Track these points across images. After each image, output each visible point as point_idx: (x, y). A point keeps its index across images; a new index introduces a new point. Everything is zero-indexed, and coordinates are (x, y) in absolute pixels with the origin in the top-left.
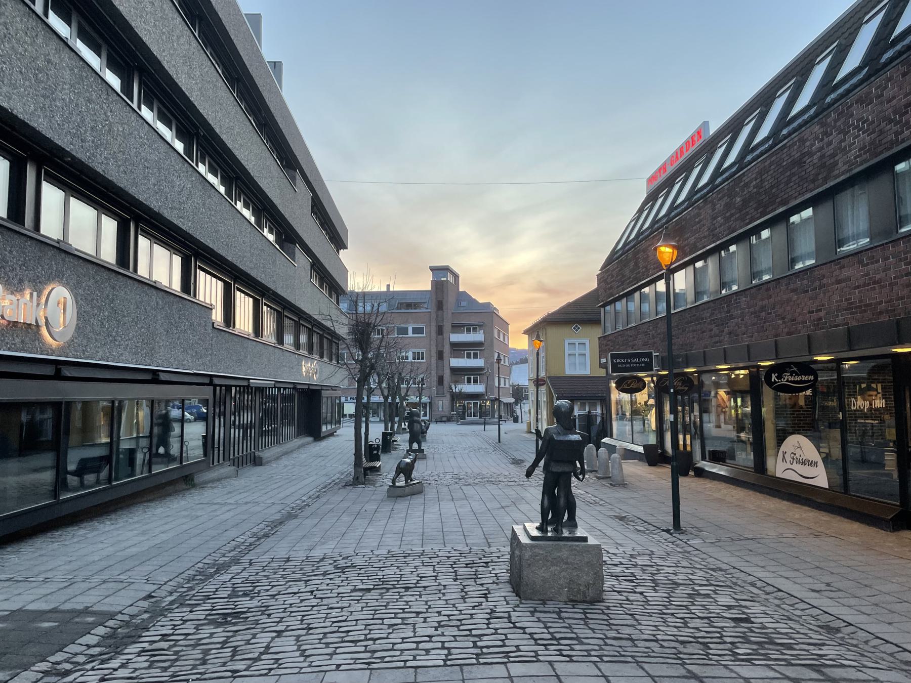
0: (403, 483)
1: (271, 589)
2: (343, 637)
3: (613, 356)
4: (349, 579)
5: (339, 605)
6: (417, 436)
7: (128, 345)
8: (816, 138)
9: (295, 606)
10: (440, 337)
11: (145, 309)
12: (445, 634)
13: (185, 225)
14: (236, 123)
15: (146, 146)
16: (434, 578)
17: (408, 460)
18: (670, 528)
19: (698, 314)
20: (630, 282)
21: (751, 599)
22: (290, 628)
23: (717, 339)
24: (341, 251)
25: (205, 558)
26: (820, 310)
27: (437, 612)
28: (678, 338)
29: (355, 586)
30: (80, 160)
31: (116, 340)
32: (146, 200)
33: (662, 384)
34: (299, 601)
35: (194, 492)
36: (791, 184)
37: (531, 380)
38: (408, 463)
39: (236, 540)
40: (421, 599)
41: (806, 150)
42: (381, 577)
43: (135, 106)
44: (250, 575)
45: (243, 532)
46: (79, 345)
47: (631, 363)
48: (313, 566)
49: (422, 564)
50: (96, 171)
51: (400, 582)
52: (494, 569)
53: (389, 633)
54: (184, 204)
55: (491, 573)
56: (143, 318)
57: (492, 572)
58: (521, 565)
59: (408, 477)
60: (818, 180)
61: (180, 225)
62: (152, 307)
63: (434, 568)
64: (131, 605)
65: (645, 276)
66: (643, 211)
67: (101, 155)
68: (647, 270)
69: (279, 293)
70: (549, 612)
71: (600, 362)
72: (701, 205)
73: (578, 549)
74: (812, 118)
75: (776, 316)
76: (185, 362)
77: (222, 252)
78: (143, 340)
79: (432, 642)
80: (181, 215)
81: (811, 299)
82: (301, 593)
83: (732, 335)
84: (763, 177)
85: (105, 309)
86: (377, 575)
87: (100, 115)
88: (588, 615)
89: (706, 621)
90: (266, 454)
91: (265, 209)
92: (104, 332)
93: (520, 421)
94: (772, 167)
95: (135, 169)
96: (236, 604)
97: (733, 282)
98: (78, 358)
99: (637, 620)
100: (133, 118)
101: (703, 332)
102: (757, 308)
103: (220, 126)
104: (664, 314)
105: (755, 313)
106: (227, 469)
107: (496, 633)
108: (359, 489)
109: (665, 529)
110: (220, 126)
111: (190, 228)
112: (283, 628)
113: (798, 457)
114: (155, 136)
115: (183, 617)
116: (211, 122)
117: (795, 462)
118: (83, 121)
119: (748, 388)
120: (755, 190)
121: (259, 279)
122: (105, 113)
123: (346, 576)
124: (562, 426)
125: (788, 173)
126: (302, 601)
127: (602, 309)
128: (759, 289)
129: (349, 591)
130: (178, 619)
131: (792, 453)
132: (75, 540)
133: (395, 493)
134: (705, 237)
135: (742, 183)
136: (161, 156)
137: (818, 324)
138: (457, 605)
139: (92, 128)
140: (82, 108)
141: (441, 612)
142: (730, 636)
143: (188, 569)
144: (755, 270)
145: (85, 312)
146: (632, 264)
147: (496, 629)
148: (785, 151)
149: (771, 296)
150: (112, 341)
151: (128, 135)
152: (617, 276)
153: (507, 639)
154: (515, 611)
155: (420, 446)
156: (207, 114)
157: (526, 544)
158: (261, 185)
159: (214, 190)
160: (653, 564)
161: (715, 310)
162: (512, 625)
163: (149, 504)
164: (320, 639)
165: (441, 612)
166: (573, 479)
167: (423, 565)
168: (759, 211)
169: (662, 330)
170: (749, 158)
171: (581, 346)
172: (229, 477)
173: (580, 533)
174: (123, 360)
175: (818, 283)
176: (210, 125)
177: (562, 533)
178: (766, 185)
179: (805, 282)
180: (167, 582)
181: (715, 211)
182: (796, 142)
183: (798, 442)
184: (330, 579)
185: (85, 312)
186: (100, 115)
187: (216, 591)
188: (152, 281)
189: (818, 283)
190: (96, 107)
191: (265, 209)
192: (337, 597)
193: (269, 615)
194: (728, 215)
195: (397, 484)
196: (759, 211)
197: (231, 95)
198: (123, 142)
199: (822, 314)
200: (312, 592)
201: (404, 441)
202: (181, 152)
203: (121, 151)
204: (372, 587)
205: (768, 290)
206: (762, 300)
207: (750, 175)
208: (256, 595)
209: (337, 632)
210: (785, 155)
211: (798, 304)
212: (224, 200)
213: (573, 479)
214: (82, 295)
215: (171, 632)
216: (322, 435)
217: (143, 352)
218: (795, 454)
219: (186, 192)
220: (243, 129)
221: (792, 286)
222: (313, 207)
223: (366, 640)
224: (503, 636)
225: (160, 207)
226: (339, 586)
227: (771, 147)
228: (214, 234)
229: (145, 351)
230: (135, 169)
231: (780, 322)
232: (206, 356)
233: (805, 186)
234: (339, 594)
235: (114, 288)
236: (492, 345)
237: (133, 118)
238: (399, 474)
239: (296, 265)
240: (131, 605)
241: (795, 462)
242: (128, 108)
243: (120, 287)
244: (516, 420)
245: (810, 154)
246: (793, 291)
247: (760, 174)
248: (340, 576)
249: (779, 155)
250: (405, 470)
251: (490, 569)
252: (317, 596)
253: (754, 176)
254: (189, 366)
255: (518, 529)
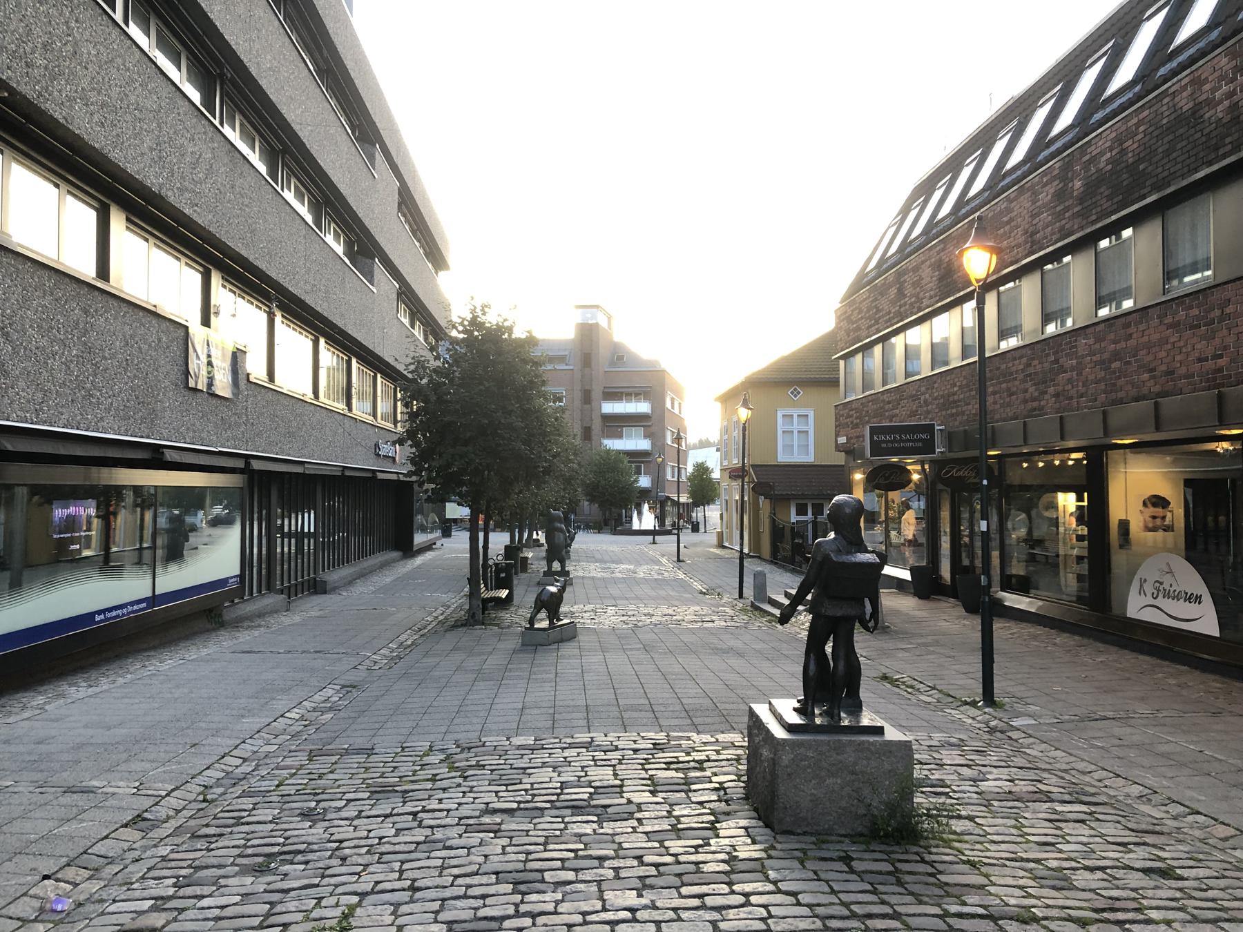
0: (545, 624)
1: (346, 805)
2: (476, 909)
3: (874, 431)
4: (475, 789)
5: (462, 842)
6: (558, 551)
7: (112, 404)
8: (1222, 78)
9: (388, 843)
10: (587, 406)
11: (140, 348)
12: (658, 904)
13: (202, 218)
14: (282, 62)
15: (137, 84)
16: (618, 790)
17: (553, 589)
18: (978, 699)
19: (1003, 367)
20: (890, 320)
21: (1151, 828)
22: (380, 887)
23: (1035, 404)
24: (441, 274)
25: (236, 747)
26: (1221, 356)
27: (635, 858)
28: (969, 404)
29: (487, 804)
30: (24, 97)
31: (91, 395)
32: (138, 172)
33: (948, 472)
34: (393, 831)
35: (223, 635)
36: (1175, 155)
37: (725, 470)
38: (552, 594)
39: (286, 715)
40: (602, 831)
41: (1204, 97)
42: (529, 786)
43: (118, 16)
44: (310, 780)
45: (298, 702)
46: (29, 402)
47: (901, 441)
48: (414, 763)
49: (592, 763)
50: (51, 116)
51: (563, 797)
52: (715, 774)
53: (557, 903)
54: (201, 183)
55: (711, 782)
56: (136, 362)
57: (714, 779)
58: (774, 775)
59: (554, 614)
60: (1225, 145)
61: (195, 217)
62: (150, 346)
63: (614, 770)
64: (106, 837)
65: (915, 310)
66: (910, 210)
67: (60, 91)
68: (920, 300)
69: (350, 332)
70: (831, 859)
71: (836, 441)
72: (1012, 196)
73: (872, 748)
74: (1214, 46)
75: (1139, 367)
76: (204, 435)
77: (262, 264)
78: (137, 398)
79: (638, 921)
80: (196, 202)
81: (1203, 338)
82: (395, 815)
83: (1061, 398)
84: (1126, 145)
85: (72, 345)
86: (521, 783)
87: (58, 24)
88: (898, 865)
89: (1099, 875)
90: (334, 576)
91: (328, 203)
92: (71, 381)
93: (702, 529)
94: (1142, 129)
95: (119, 121)
96: (289, 833)
97: (1126, 294)
98: (26, 422)
99: (987, 876)
100: (113, 36)
101: (1011, 394)
102: (1106, 356)
103: (258, 64)
104: (976, 359)
105: (1102, 362)
106: (271, 600)
107: (747, 904)
108: (478, 631)
109: (968, 700)
110: (258, 64)
111: (211, 222)
112: (368, 887)
113: (1168, 588)
114: (151, 70)
115: (194, 860)
116: (242, 57)
117: (1161, 595)
118: (29, 32)
119: (1084, 482)
120: (1109, 167)
121: (318, 309)
122: (67, 23)
123: (471, 784)
124: (844, 537)
125: (1171, 137)
126: (398, 832)
127: (842, 363)
128: (1112, 325)
129: (477, 813)
130: (185, 864)
131: (1157, 581)
132: (26, 715)
133: (534, 642)
134: (1018, 246)
135: (1087, 157)
136: (163, 104)
137: (1215, 379)
138: (667, 844)
139: (44, 46)
140: (26, 10)
141: (642, 857)
142: (1056, 859)
143: (208, 768)
144: (1004, 328)
145: (37, 348)
146: (893, 291)
147: (747, 895)
148: (1166, 101)
149: (1131, 335)
150: (84, 397)
151: (106, 63)
152: (868, 311)
153: (771, 916)
154: (770, 857)
155: (563, 566)
156: (236, 44)
157: (783, 739)
158: (322, 164)
159: (247, 166)
160: (971, 763)
161: (1033, 359)
162: (771, 887)
163: (152, 653)
164: (437, 912)
165: (642, 857)
166: (857, 624)
167: (596, 765)
168: (1115, 200)
169: (941, 393)
170: (1098, 116)
171: (802, 419)
172: (276, 612)
173: (866, 720)
174: (103, 428)
175: (1217, 313)
176: (242, 61)
177: (840, 719)
178: (1130, 158)
179: (1195, 312)
180: (173, 790)
181: (1038, 204)
182: (1186, 84)
183: (1168, 564)
184: (444, 790)
185: (37, 348)
186: (58, 24)
187: (254, 809)
188: (150, 304)
189: (1217, 313)
190: (50, 11)
191: (328, 203)
192: (457, 824)
193: (344, 859)
194: (1058, 209)
195: (536, 626)
196: (1115, 200)
197: (274, 17)
198: (98, 73)
199: (1222, 362)
200: (415, 814)
201: (538, 559)
202: (198, 102)
203: (94, 89)
204: (515, 805)
205: (1127, 325)
206: (1115, 342)
207: (1100, 143)
208: (321, 817)
209: (465, 897)
210: (1165, 108)
211: (1180, 348)
212: (264, 182)
213: (857, 624)
214: (31, 320)
215: (171, 891)
216: (415, 549)
217: (137, 417)
218: (1161, 583)
219: (203, 166)
220: (293, 73)
221: (1168, 320)
222: (400, 204)
223: (517, 914)
224: (762, 910)
225: (161, 185)
226: (460, 804)
227: (1139, 97)
228: (249, 235)
229: (140, 414)
230: (119, 121)
231: (1146, 376)
232: (238, 425)
233: (1160, 169)
234: (460, 819)
235: (86, 312)
236: (662, 419)
237: (113, 36)
238: (538, 612)
239: (375, 291)
240: (106, 837)
241: (1161, 595)
242: (105, 17)
243: (96, 311)
244: (695, 529)
245: (1212, 103)
246: (1170, 326)
247: (1120, 140)
248: (459, 785)
249: (1154, 108)
250: (551, 605)
251: (708, 773)
252: (426, 823)
253: (1108, 144)
254: (211, 440)
255: (762, 710)
